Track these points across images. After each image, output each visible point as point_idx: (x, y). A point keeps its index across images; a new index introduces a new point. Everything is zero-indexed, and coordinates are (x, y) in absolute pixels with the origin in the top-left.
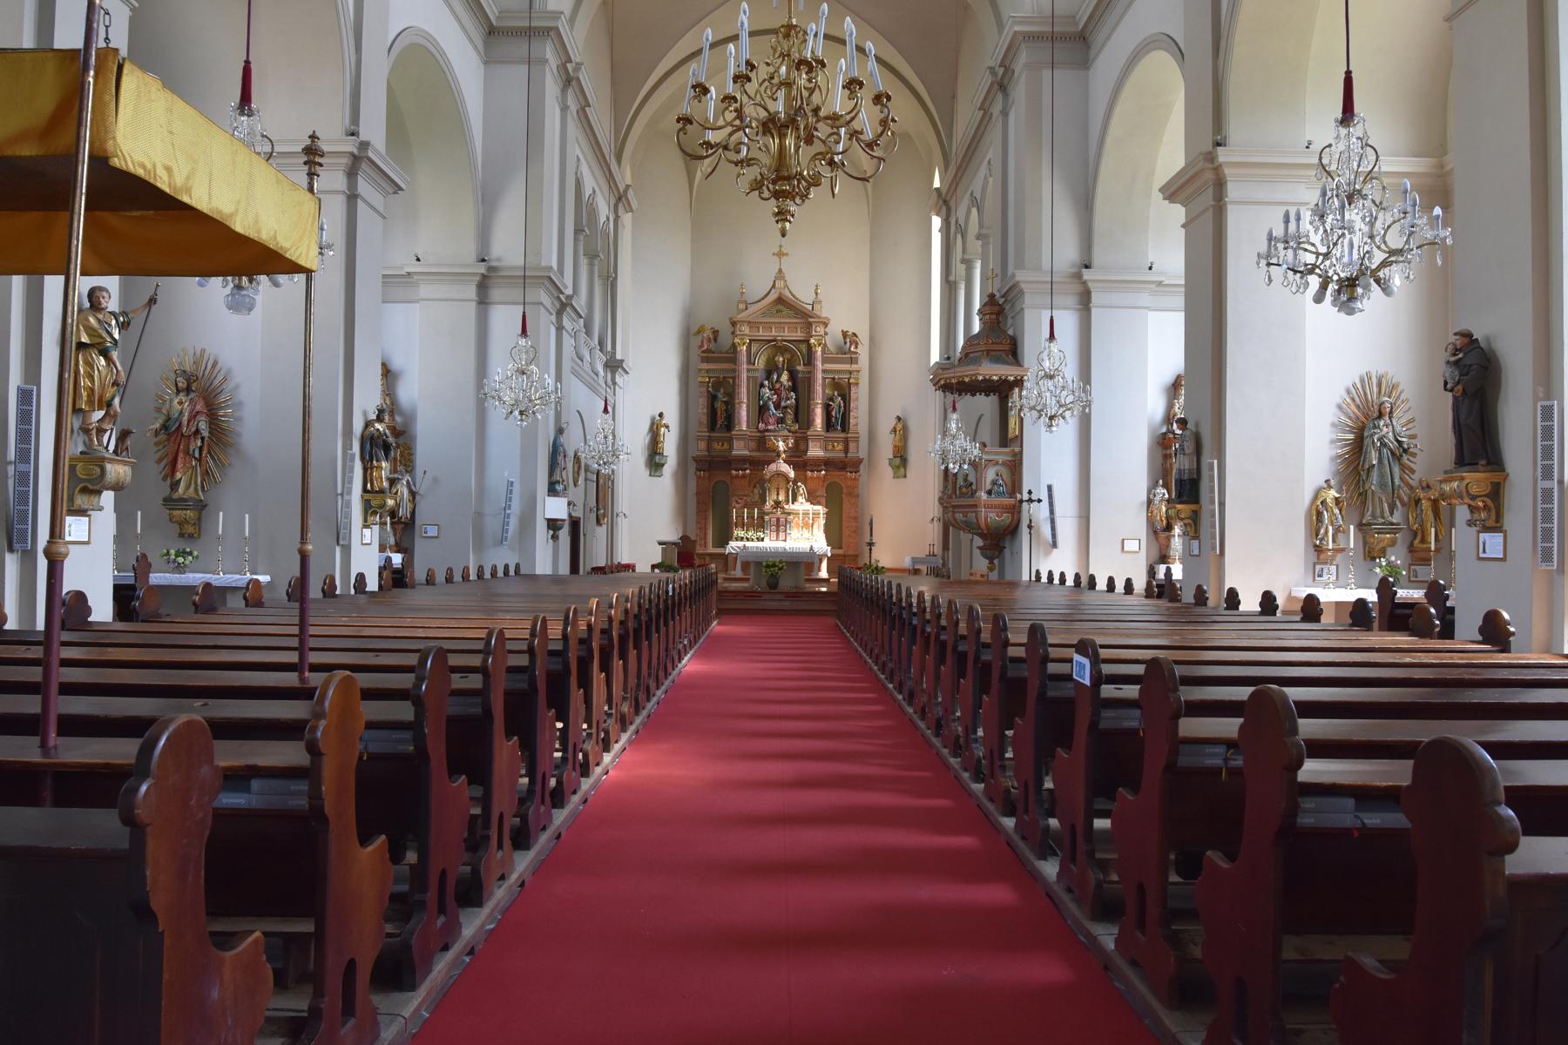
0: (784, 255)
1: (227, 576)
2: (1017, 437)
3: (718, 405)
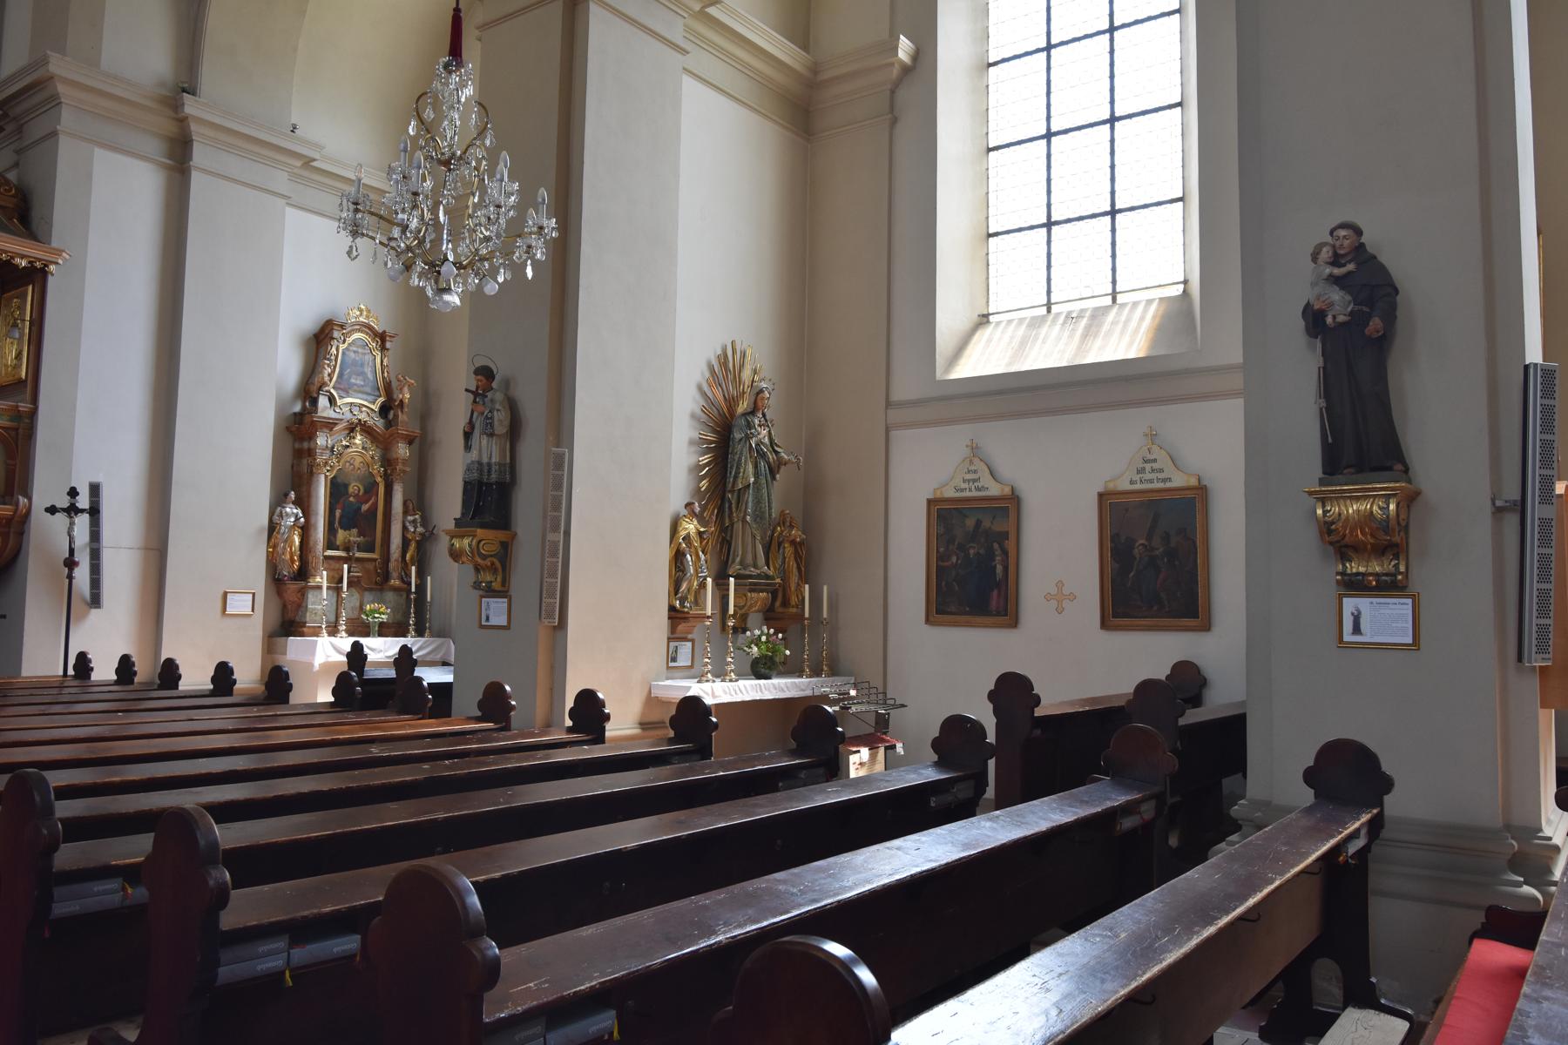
2: (21, 383)
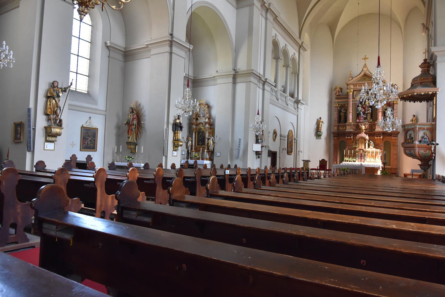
0: (367, 58)
1: (122, 163)
3: (342, 114)
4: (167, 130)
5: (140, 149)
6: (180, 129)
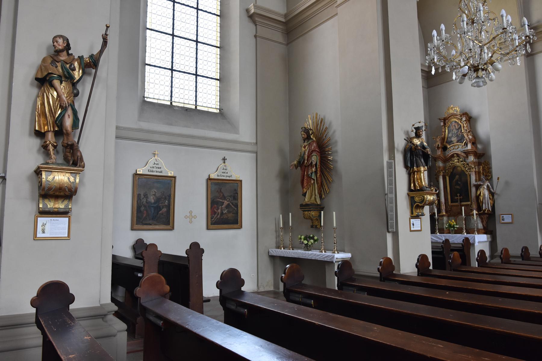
4: (391, 166)
5: (329, 218)
6: (423, 160)
